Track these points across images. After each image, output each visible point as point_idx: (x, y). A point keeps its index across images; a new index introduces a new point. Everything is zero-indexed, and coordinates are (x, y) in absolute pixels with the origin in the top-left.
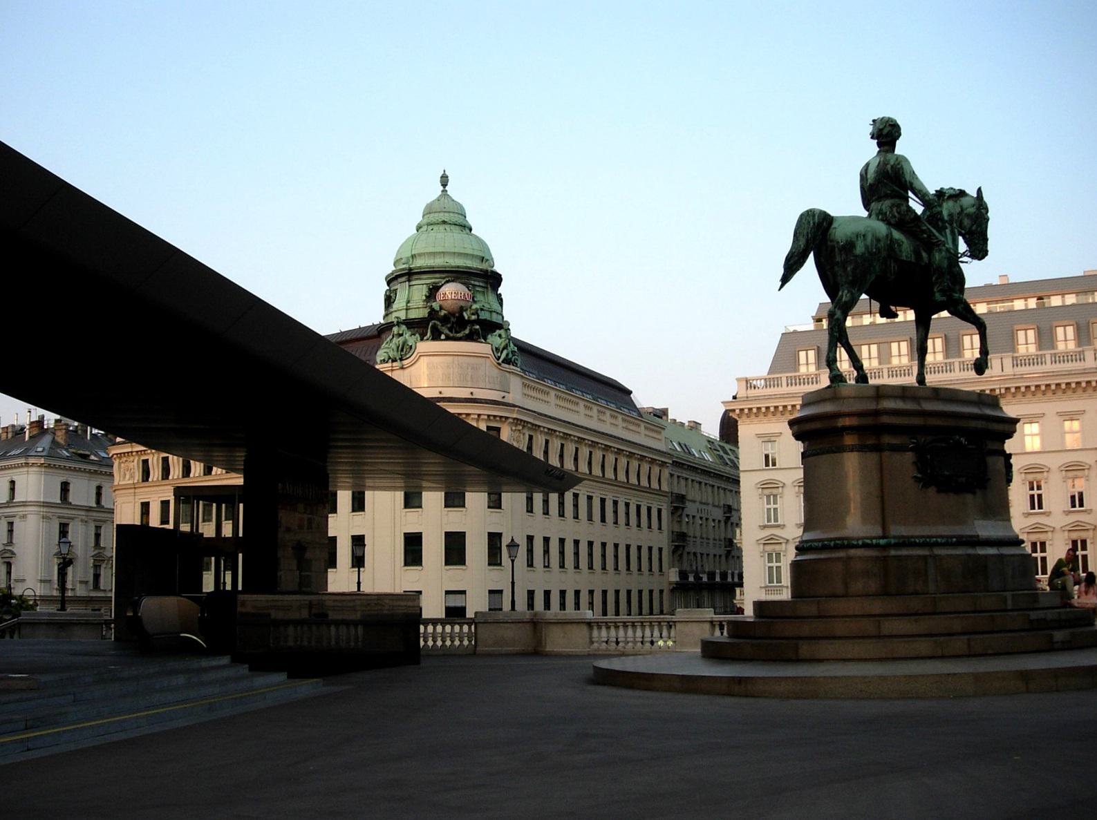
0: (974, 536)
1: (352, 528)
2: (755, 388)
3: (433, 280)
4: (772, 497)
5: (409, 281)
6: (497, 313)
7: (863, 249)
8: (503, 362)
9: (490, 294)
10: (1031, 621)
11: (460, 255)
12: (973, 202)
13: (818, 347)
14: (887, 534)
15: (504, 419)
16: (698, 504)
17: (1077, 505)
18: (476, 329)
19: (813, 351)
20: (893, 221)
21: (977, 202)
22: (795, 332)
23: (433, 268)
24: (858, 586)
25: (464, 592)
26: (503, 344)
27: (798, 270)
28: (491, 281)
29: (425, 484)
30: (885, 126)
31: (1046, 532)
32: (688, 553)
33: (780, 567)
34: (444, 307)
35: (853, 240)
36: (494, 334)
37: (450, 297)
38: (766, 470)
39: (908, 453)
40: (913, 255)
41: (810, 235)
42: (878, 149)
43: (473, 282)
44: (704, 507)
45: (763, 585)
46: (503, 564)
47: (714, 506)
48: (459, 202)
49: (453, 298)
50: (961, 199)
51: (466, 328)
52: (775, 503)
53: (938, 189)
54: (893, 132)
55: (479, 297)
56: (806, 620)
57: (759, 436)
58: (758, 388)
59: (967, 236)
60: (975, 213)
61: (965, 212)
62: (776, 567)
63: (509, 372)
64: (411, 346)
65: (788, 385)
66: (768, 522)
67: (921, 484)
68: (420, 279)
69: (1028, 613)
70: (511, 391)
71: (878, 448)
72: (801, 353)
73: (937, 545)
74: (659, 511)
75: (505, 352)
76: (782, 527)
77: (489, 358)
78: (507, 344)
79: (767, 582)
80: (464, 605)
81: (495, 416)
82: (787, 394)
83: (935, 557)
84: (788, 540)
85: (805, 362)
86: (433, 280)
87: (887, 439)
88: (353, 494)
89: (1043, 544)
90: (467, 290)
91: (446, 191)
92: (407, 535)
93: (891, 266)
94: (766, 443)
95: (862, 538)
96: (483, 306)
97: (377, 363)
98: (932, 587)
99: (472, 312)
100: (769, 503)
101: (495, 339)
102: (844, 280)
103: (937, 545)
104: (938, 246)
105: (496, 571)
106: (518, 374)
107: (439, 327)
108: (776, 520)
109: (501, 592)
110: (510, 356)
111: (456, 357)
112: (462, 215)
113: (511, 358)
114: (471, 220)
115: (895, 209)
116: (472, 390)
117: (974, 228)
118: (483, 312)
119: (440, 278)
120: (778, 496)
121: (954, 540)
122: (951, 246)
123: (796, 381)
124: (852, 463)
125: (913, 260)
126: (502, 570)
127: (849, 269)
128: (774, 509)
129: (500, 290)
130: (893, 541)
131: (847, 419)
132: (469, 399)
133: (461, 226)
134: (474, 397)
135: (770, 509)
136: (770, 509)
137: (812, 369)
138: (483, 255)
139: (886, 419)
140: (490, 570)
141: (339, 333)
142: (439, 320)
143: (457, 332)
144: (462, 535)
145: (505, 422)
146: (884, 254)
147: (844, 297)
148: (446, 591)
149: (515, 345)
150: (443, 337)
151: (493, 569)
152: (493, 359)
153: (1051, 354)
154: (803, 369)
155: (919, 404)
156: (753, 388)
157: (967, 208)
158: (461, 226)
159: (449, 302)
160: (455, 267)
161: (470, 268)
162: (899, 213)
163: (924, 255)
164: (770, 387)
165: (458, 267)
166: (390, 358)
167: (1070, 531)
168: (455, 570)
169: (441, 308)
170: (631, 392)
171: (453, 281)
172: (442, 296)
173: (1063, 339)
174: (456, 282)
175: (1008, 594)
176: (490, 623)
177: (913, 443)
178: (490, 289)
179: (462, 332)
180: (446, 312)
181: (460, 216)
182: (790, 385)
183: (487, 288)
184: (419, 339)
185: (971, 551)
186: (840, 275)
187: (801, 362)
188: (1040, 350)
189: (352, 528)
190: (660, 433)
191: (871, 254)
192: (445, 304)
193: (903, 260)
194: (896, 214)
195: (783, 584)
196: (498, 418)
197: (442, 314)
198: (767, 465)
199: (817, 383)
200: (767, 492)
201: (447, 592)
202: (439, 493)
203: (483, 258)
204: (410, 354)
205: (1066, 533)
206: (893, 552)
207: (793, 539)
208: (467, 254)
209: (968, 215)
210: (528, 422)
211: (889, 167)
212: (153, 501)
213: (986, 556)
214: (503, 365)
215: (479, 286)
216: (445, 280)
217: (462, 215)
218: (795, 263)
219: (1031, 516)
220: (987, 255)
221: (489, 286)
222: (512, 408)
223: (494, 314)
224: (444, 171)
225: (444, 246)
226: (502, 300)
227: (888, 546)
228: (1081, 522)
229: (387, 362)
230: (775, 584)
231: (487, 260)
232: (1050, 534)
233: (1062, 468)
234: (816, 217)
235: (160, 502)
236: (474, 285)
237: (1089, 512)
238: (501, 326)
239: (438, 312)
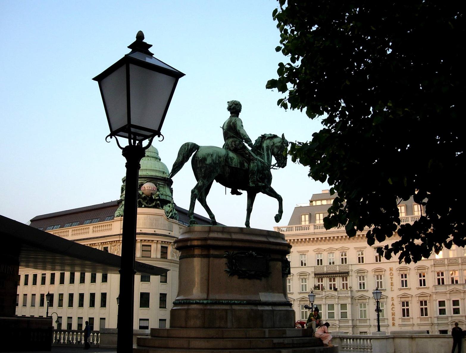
0: (258, 301)
1: (41, 291)
2: (283, 231)
3: (141, 181)
4: (304, 279)
6: (169, 196)
7: (211, 161)
8: (170, 218)
9: (166, 188)
10: (275, 344)
11: (153, 170)
12: (279, 140)
13: (310, 214)
14: (208, 298)
15: (169, 243)
17: (423, 285)
18: (158, 203)
19: (308, 215)
20: (232, 149)
21: (282, 140)
22: (301, 207)
23: (141, 176)
24: (191, 323)
25: (148, 320)
26: (170, 210)
27: (179, 170)
28: (167, 182)
29: (86, 270)
30: (232, 105)
31: (384, 298)
33: (366, 310)
34: (144, 193)
35: (206, 157)
36: (167, 205)
37: (147, 189)
39: (223, 259)
40: (239, 165)
41: (185, 155)
42: (230, 115)
43: (158, 182)
45: (419, 317)
46: (166, 308)
48: (155, 147)
49: (148, 189)
50: (274, 139)
51: (153, 203)
52: (305, 282)
53: (263, 134)
54: (236, 107)
55: (161, 189)
56: (170, 339)
57: (355, 248)
58: (285, 231)
59: (276, 157)
60: (280, 145)
61: (275, 145)
63: (173, 222)
65: (296, 230)
66: (302, 291)
67: (229, 274)
69: (272, 339)
70: (173, 231)
71: (207, 256)
72: (302, 216)
73: (234, 304)
77: (163, 216)
78: (172, 210)
79: (360, 317)
80: (148, 325)
82: (296, 234)
83: (232, 310)
84: (294, 300)
85: (304, 220)
86: (141, 181)
87: (212, 252)
88: (103, 275)
89: (407, 303)
90: (155, 186)
93: (226, 170)
94: (302, 255)
95: (195, 300)
96: (163, 193)
97: (115, 217)
98: (229, 325)
99: (157, 195)
100: (302, 282)
101: (167, 208)
102: (200, 176)
103: (234, 304)
104: (253, 160)
105: (163, 311)
106: (178, 224)
107: (142, 202)
108: (306, 290)
109: (165, 320)
110: (174, 215)
111: (148, 215)
112: (156, 153)
113: (174, 216)
114: (160, 156)
115: (233, 143)
116: (155, 230)
117: (279, 152)
118: (162, 196)
119: (144, 180)
120: (307, 279)
121: (245, 302)
122: (266, 161)
123: (301, 229)
124: (197, 263)
125: (239, 167)
126: (166, 310)
127: (203, 170)
128: (305, 285)
129: (172, 187)
130: (209, 302)
131: (196, 241)
132: (154, 234)
133: (155, 158)
134: (156, 233)
135: (303, 285)
136: (303, 285)
137: (307, 223)
138: (164, 171)
139: (210, 242)
140: (160, 310)
141: (103, 204)
142: (142, 198)
143: (149, 204)
144: (148, 294)
145: (170, 244)
146: (223, 164)
147: (200, 184)
148: (140, 319)
149: (176, 210)
150: (143, 206)
151: (162, 310)
152: (165, 217)
153: (411, 217)
154: (303, 223)
155: (231, 236)
156: (282, 231)
157: (276, 143)
158: (155, 158)
159: (146, 191)
160: (150, 176)
161: (158, 176)
162: (235, 145)
163: (246, 164)
164: (299, 230)
165: (152, 176)
166: (120, 215)
167: (419, 297)
168: (144, 310)
169: (143, 193)
171: (149, 182)
172: (143, 188)
173: (417, 210)
174: (151, 182)
175: (267, 330)
176: (106, 333)
177: (227, 254)
178: (166, 186)
179: (152, 204)
180: (145, 195)
181: (155, 154)
182: (297, 230)
183: (165, 185)
185: (254, 308)
186: (199, 173)
187: (302, 220)
188: (407, 215)
189: (80, 290)
191: (215, 163)
192: (145, 192)
193: (233, 167)
194: (234, 145)
195: (335, 319)
196: (166, 243)
197: (143, 196)
198: (302, 265)
199: (308, 229)
200: (302, 277)
201: (140, 320)
202: (100, 274)
203: (164, 172)
205: (418, 298)
206: (209, 307)
207: (297, 299)
208: (157, 170)
209: (277, 147)
211: (232, 123)
212: (22, 275)
213: (262, 311)
214: (170, 219)
215: (162, 184)
216: (146, 181)
217: (156, 153)
218: (177, 167)
219: (359, 292)
220: (286, 165)
221: (166, 184)
222: (173, 238)
223: (168, 197)
225: (147, 167)
226: (172, 191)
227: (207, 304)
228: (424, 293)
229: (119, 217)
231: (166, 173)
232: (410, 298)
233: (398, 270)
234: (189, 146)
235: (24, 275)
236: (159, 184)
237: (428, 288)
239: (141, 195)
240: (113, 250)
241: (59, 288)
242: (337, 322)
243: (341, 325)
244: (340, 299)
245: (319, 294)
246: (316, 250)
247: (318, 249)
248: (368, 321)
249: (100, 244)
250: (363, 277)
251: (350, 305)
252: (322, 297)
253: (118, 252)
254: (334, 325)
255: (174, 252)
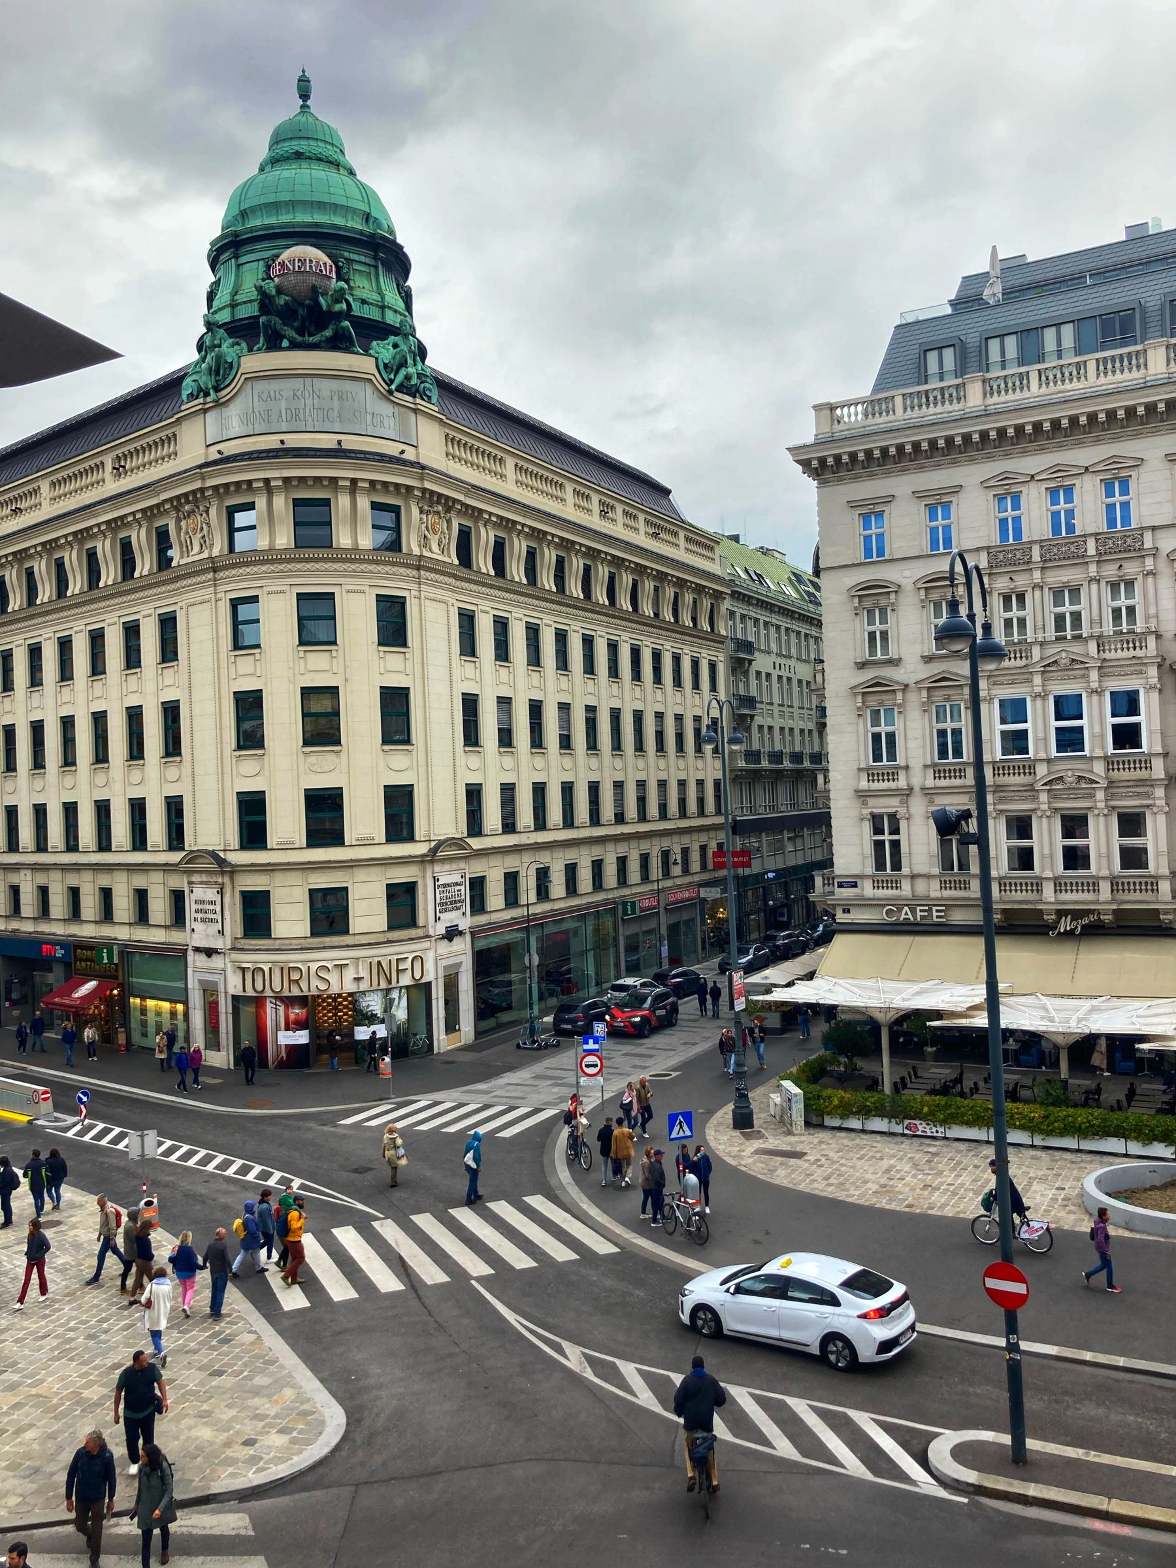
5: (237, 257)
6: (396, 311)
8: (397, 390)
16: (773, 656)
32: (761, 727)
38: (866, 564)
43: (346, 254)
44: (783, 661)
47: (799, 659)
52: (883, 620)
57: (918, 495)
62: (1013, 518)
64: (231, 364)
68: (253, 251)
74: (713, 666)
75: (403, 372)
76: (895, 662)
81: (385, 484)
84: (907, 686)
91: (308, 107)
92: (239, 696)
101: (384, 350)
110: (414, 381)
142: (279, 314)
143: (310, 335)
150: (285, 343)
169: (280, 290)
170: (666, 492)
184: (245, 350)
190: (711, 549)
195: (1087, 752)
197: (282, 302)
204: (231, 377)
210: (455, 500)
214: (396, 394)
224: (303, 71)
230: (885, 762)
238: (405, 331)
240: (187, 533)
241: (124, 684)
242: (1099, 768)
243: (1115, 775)
244: (1106, 670)
245: (1018, 655)
246: (991, 483)
247: (1006, 477)
248: (902, 775)
249: (138, 516)
250: (1018, 596)
251: (1155, 696)
252: (1026, 666)
253: (204, 537)
254: (1084, 778)
255: (427, 528)
